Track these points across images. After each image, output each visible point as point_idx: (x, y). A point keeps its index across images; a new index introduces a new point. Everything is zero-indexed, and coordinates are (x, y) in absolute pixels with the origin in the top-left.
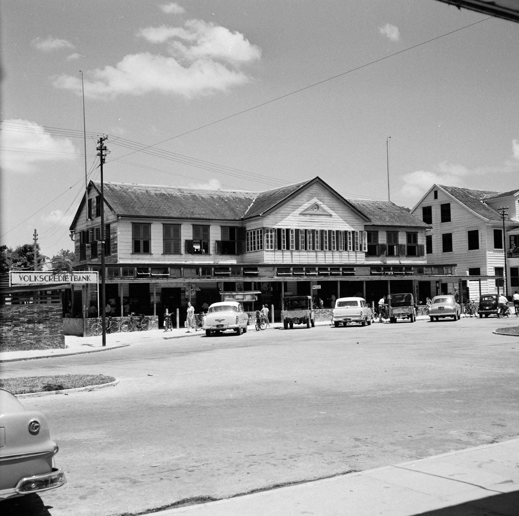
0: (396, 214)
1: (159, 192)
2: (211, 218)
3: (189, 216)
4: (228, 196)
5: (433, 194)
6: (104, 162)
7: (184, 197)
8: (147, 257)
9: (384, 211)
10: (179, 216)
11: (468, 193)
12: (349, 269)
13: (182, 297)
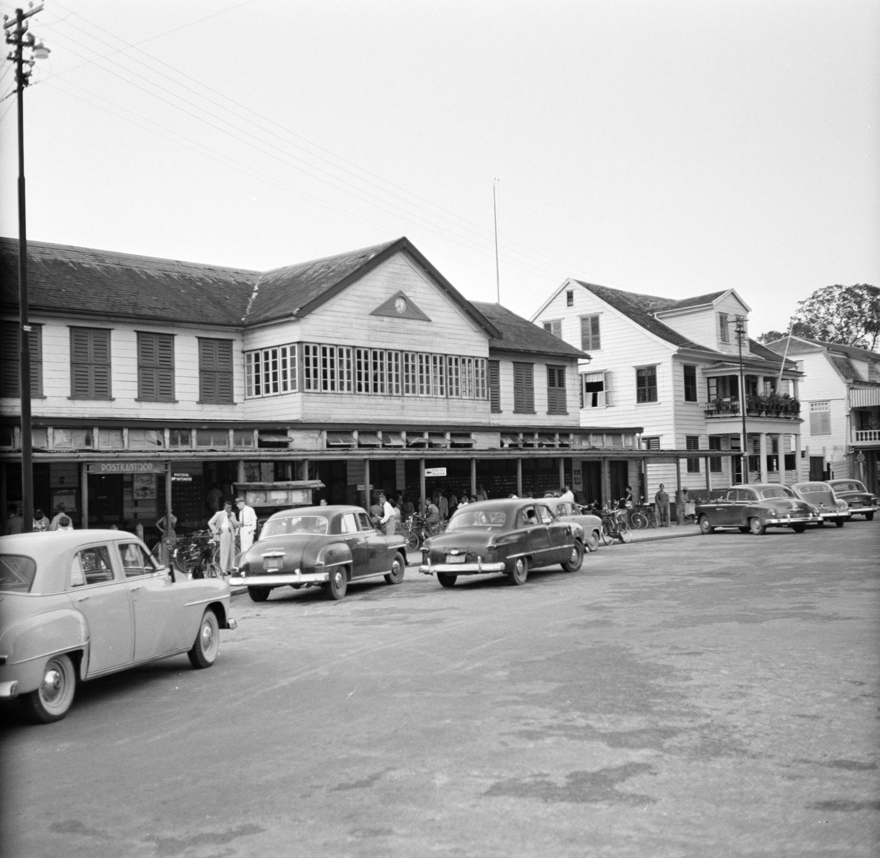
6: (27, 83)
7: (107, 269)
8: (169, 406)
10: (108, 310)
12: (462, 432)
13: (127, 498)
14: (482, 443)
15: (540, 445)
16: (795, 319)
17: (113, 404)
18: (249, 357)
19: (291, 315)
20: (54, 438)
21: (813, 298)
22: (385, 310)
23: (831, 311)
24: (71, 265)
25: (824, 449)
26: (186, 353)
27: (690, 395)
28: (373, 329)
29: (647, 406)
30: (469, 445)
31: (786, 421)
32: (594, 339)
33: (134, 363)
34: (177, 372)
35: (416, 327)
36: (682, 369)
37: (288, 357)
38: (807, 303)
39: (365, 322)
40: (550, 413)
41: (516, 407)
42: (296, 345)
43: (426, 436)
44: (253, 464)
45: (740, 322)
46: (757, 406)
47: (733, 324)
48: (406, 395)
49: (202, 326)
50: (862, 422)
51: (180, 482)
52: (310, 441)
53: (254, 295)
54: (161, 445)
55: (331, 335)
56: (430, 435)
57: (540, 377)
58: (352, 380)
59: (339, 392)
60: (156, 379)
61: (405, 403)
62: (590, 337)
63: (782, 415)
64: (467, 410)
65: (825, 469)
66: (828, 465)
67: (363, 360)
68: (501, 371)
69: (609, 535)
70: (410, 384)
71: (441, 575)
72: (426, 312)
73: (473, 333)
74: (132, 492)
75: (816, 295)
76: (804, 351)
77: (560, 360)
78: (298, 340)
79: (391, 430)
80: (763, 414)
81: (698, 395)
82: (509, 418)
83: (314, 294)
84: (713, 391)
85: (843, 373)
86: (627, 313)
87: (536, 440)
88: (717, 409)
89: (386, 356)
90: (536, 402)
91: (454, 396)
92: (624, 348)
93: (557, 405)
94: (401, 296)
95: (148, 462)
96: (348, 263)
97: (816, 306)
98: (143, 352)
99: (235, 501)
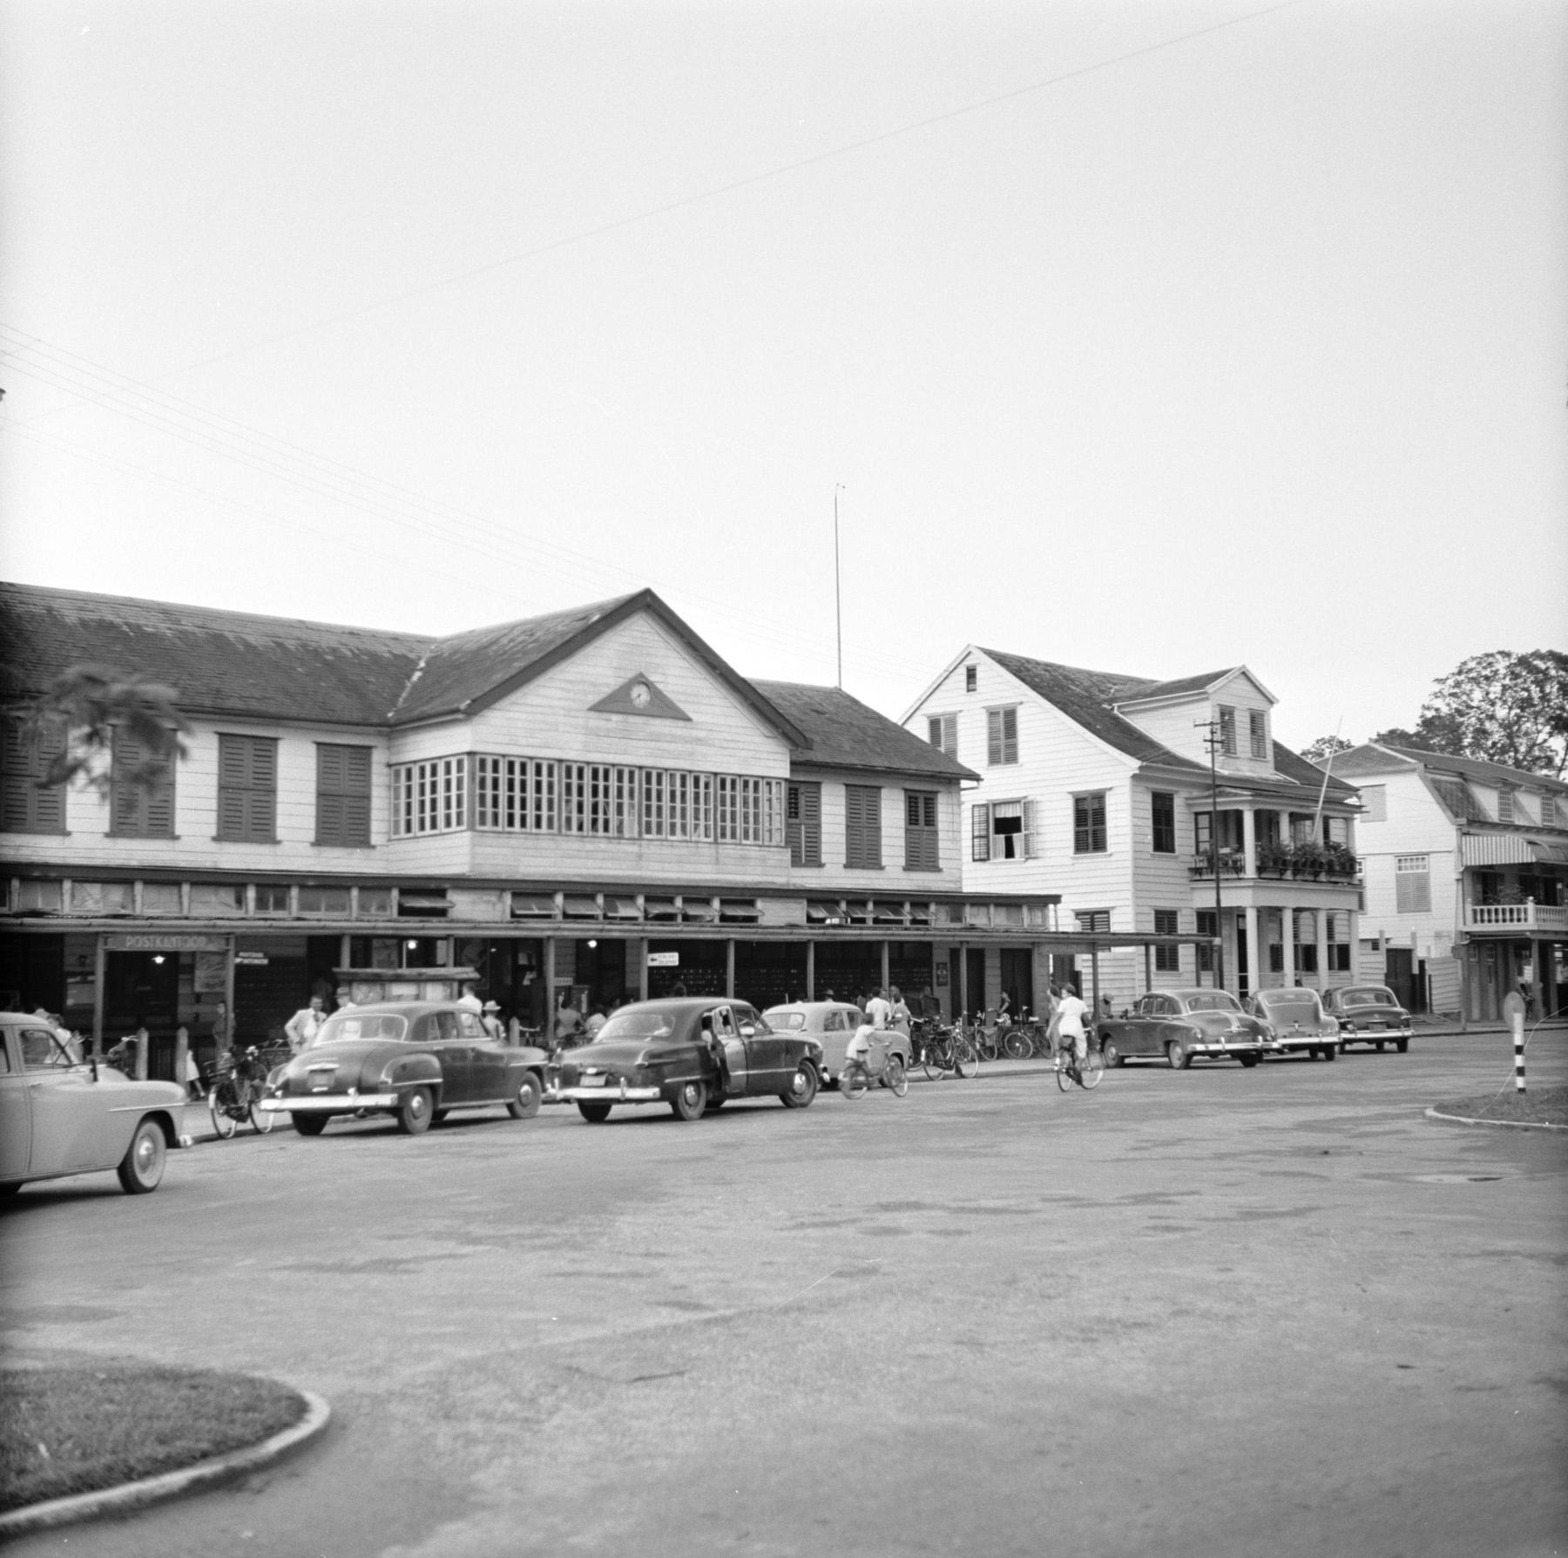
0: (871, 732)
1: (95, 616)
2: (284, 711)
3: (208, 703)
4: (334, 644)
5: (964, 678)
7: (183, 635)
8: (265, 849)
9: (834, 722)
11: (1066, 677)
12: (743, 897)
13: (183, 990)
14: (775, 917)
15: (876, 921)
16: (1428, 708)
17: (178, 845)
18: (397, 774)
19: (457, 711)
20: (73, 896)
21: (1460, 673)
22: (615, 703)
23: (1492, 696)
24: (125, 628)
25: (1414, 936)
26: (296, 768)
27: (1163, 840)
28: (594, 732)
29: (1091, 860)
30: (753, 919)
31: (1330, 887)
32: (1007, 746)
33: (213, 781)
34: (281, 796)
35: (666, 730)
36: (1148, 799)
37: (454, 776)
38: (1451, 682)
39: (581, 721)
40: (849, 865)
41: (907, 860)
42: (465, 757)
43: (679, 902)
44: (389, 942)
45: (1257, 723)
46: (1275, 862)
47: (1240, 722)
48: (646, 836)
49: (324, 726)
50: (1485, 892)
51: (248, 966)
52: (483, 907)
53: (417, 675)
54: (249, 914)
55: (523, 741)
56: (686, 901)
57: (892, 811)
58: (555, 813)
59: (534, 830)
60: (247, 811)
61: (644, 850)
62: (1002, 742)
63: (1323, 877)
64: (757, 863)
65: (1416, 971)
66: (1422, 963)
67: (574, 781)
68: (825, 799)
69: (935, 1064)
70: (654, 819)
71: (583, 1104)
72: (681, 706)
73: (762, 740)
74: (192, 981)
75: (1466, 668)
76: (1389, 769)
77: (927, 778)
78: (467, 749)
79: (619, 892)
80: (1289, 875)
81: (1177, 842)
82: (834, 874)
83: (499, 677)
84: (1205, 835)
85: (1450, 807)
86: (1064, 706)
87: (870, 913)
88: (1214, 866)
89: (613, 776)
90: (885, 851)
91: (728, 839)
92: (1060, 761)
93: (921, 855)
94: (641, 680)
95: (199, 934)
96: (560, 628)
97: (1467, 687)
98: (228, 766)
99: (334, 993)
